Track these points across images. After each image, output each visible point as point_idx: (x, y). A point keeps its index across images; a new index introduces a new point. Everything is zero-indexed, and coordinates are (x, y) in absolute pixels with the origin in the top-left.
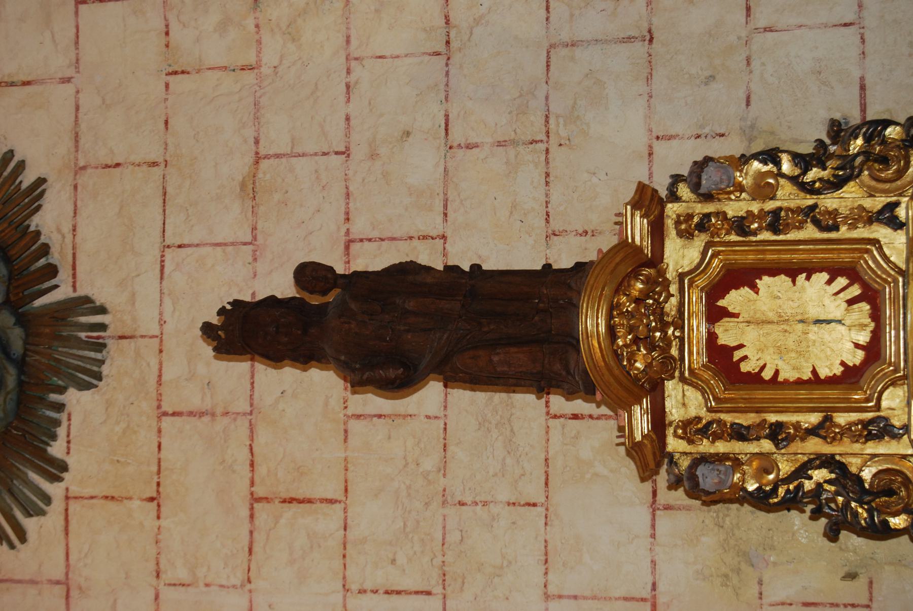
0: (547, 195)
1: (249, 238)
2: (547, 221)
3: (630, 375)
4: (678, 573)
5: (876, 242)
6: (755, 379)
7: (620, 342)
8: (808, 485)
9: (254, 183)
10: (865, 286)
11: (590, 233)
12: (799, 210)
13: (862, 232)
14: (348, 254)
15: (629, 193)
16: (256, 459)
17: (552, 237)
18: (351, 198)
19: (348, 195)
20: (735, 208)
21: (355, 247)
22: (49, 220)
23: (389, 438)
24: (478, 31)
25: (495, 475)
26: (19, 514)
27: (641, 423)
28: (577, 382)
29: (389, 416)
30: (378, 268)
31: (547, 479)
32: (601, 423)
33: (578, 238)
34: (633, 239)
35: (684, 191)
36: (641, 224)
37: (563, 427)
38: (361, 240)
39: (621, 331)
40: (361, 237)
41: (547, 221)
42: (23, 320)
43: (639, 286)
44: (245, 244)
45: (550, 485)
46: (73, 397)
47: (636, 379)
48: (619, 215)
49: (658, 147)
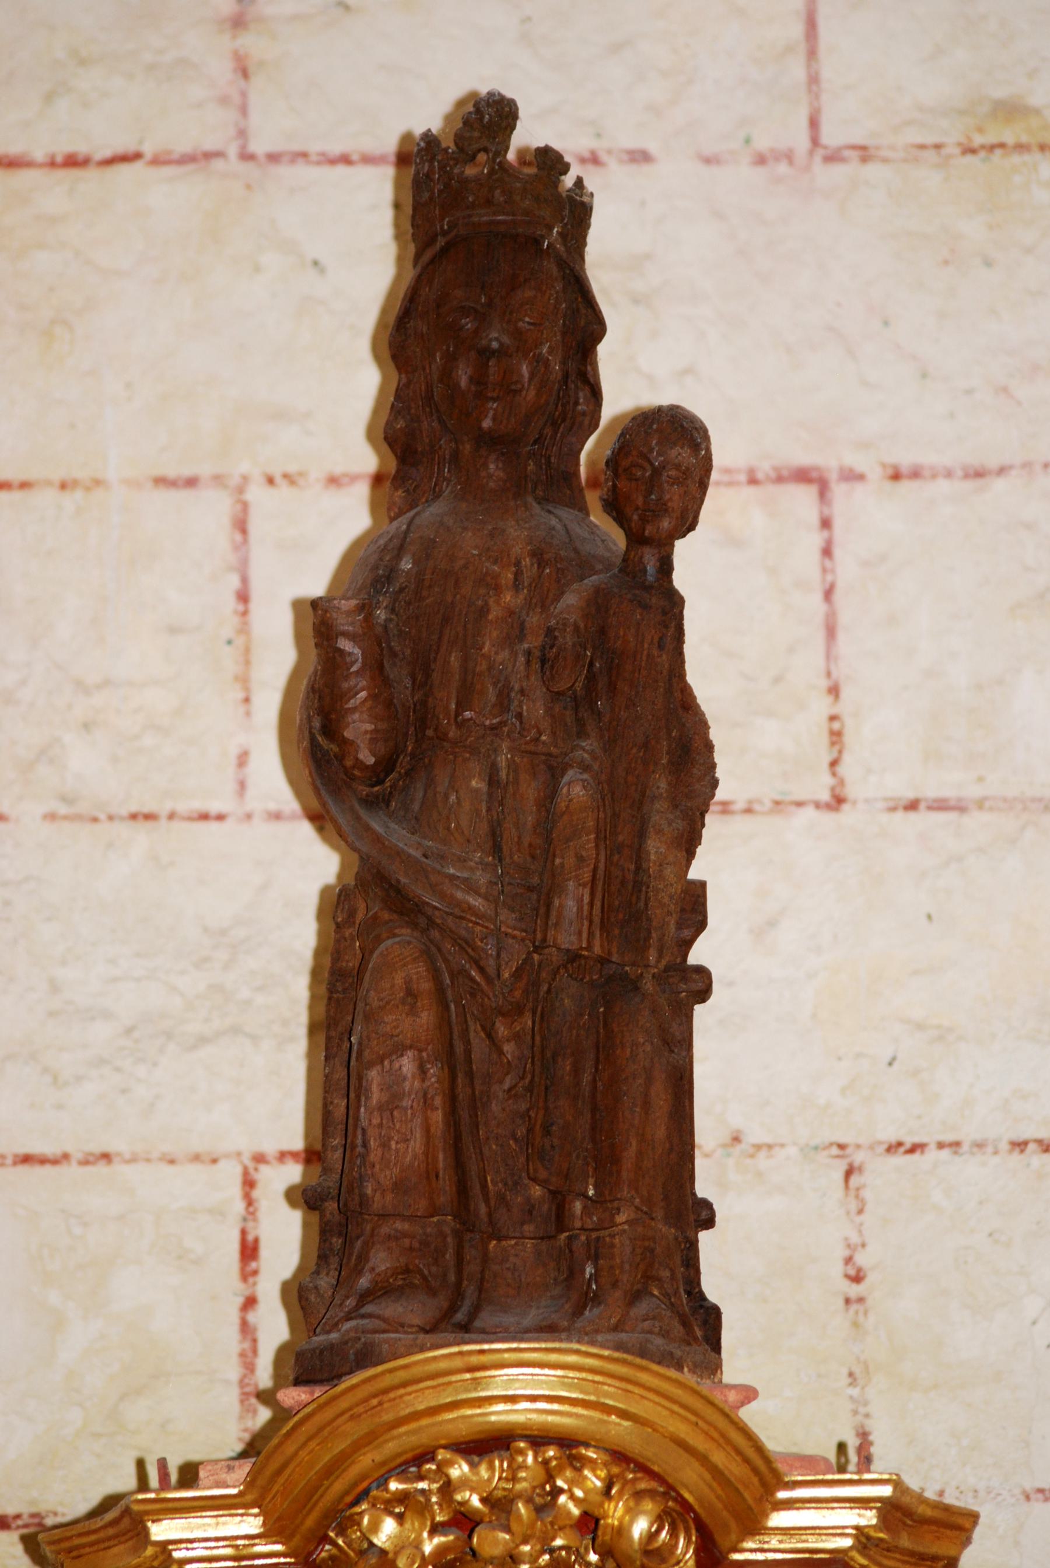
0: (980, 1145)
1: (832, 136)
2: (893, 1148)
3: (357, 1502)
7: (459, 1470)
9: (1021, 148)
11: (854, 1290)
14: (780, 479)
15: (935, 1481)
16: (91, 174)
17: (842, 1166)
18: (970, 485)
19: (979, 474)
21: (802, 500)
23: (173, 630)
25: (55, 988)
28: (335, 1326)
29: (244, 628)
30: (694, 676)
31: (43, 1161)
32: (231, 1340)
33: (842, 1253)
34: (789, 1505)
36: (837, 1531)
37: (218, 1213)
38: (826, 523)
39: (491, 1473)
40: (838, 524)
41: (893, 1148)
43: (640, 1527)
44: (814, 123)
45: (23, 1170)
47: (346, 1523)
48: (866, 1461)
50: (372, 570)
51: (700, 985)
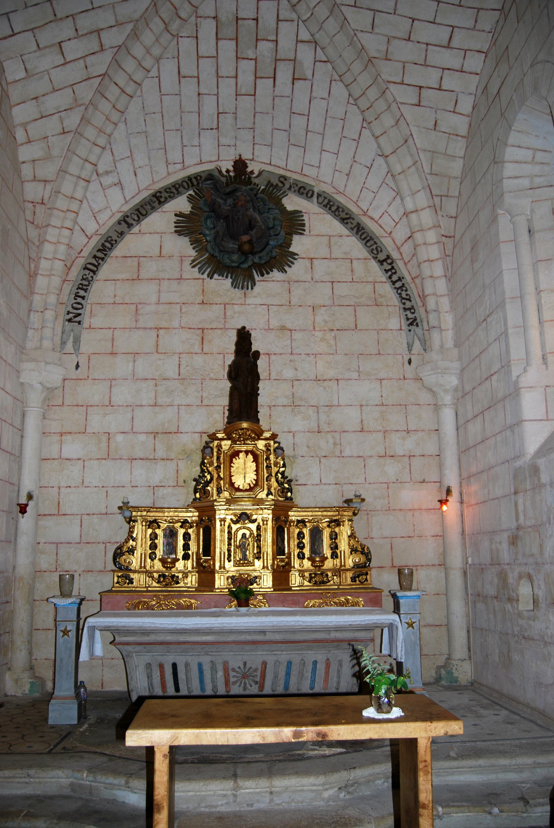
4: (185, 439)
5: (263, 490)
6: (231, 462)
8: (206, 474)
10: (253, 488)
12: (271, 472)
13: (266, 487)
20: (272, 457)
21: (267, 356)
22: (276, 274)
24: (322, 388)
26: (199, 266)
27: (220, 436)
35: (276, 445)
42: (250, 267)
46: (229, 280)
49: (292, 434)
50: (234, 362)
51: (259, 394)
